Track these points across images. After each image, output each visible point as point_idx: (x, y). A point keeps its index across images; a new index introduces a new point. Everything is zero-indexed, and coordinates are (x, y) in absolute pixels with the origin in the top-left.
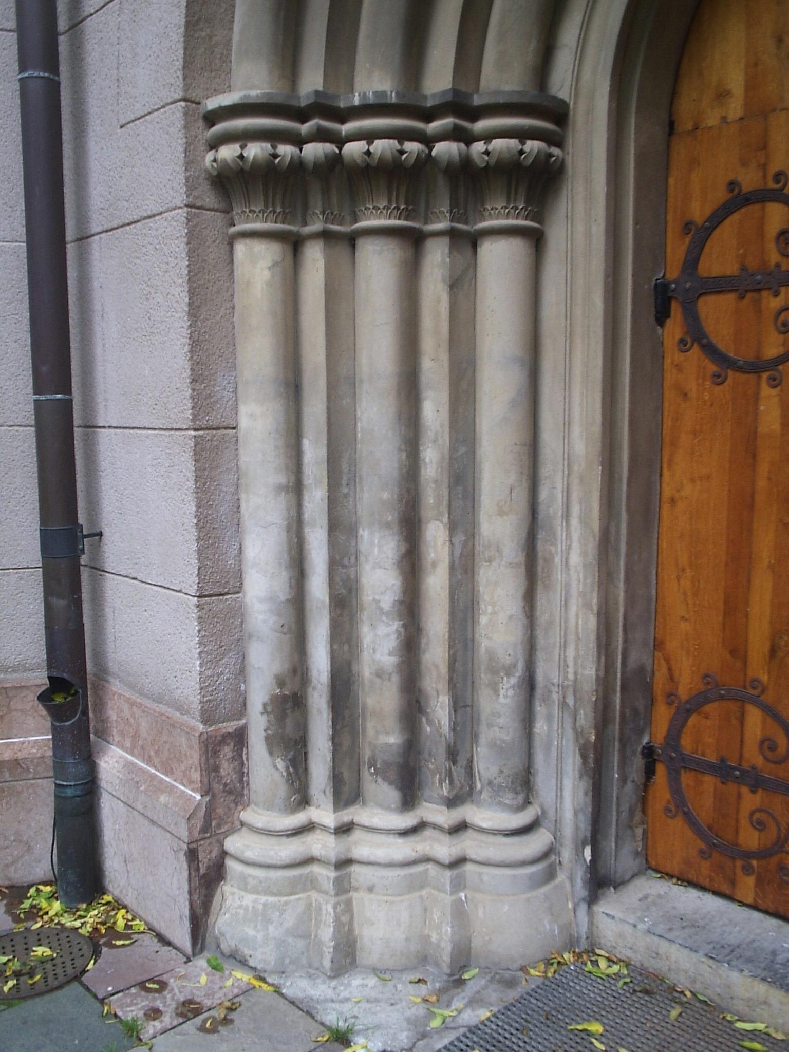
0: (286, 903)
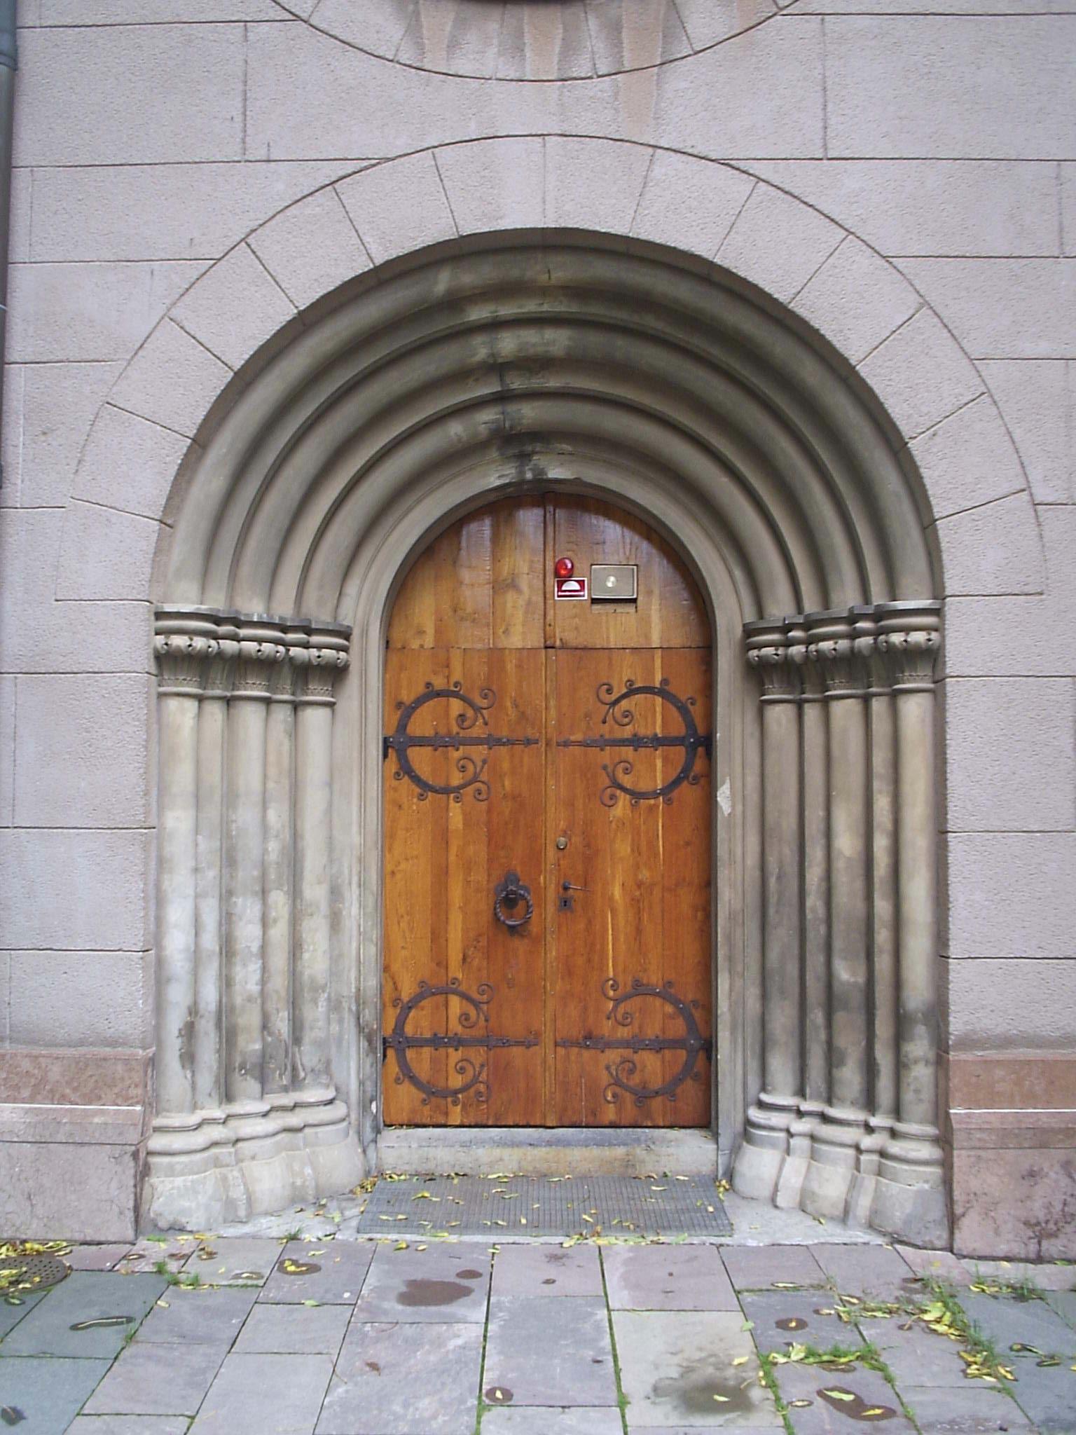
0: (205, 1177)
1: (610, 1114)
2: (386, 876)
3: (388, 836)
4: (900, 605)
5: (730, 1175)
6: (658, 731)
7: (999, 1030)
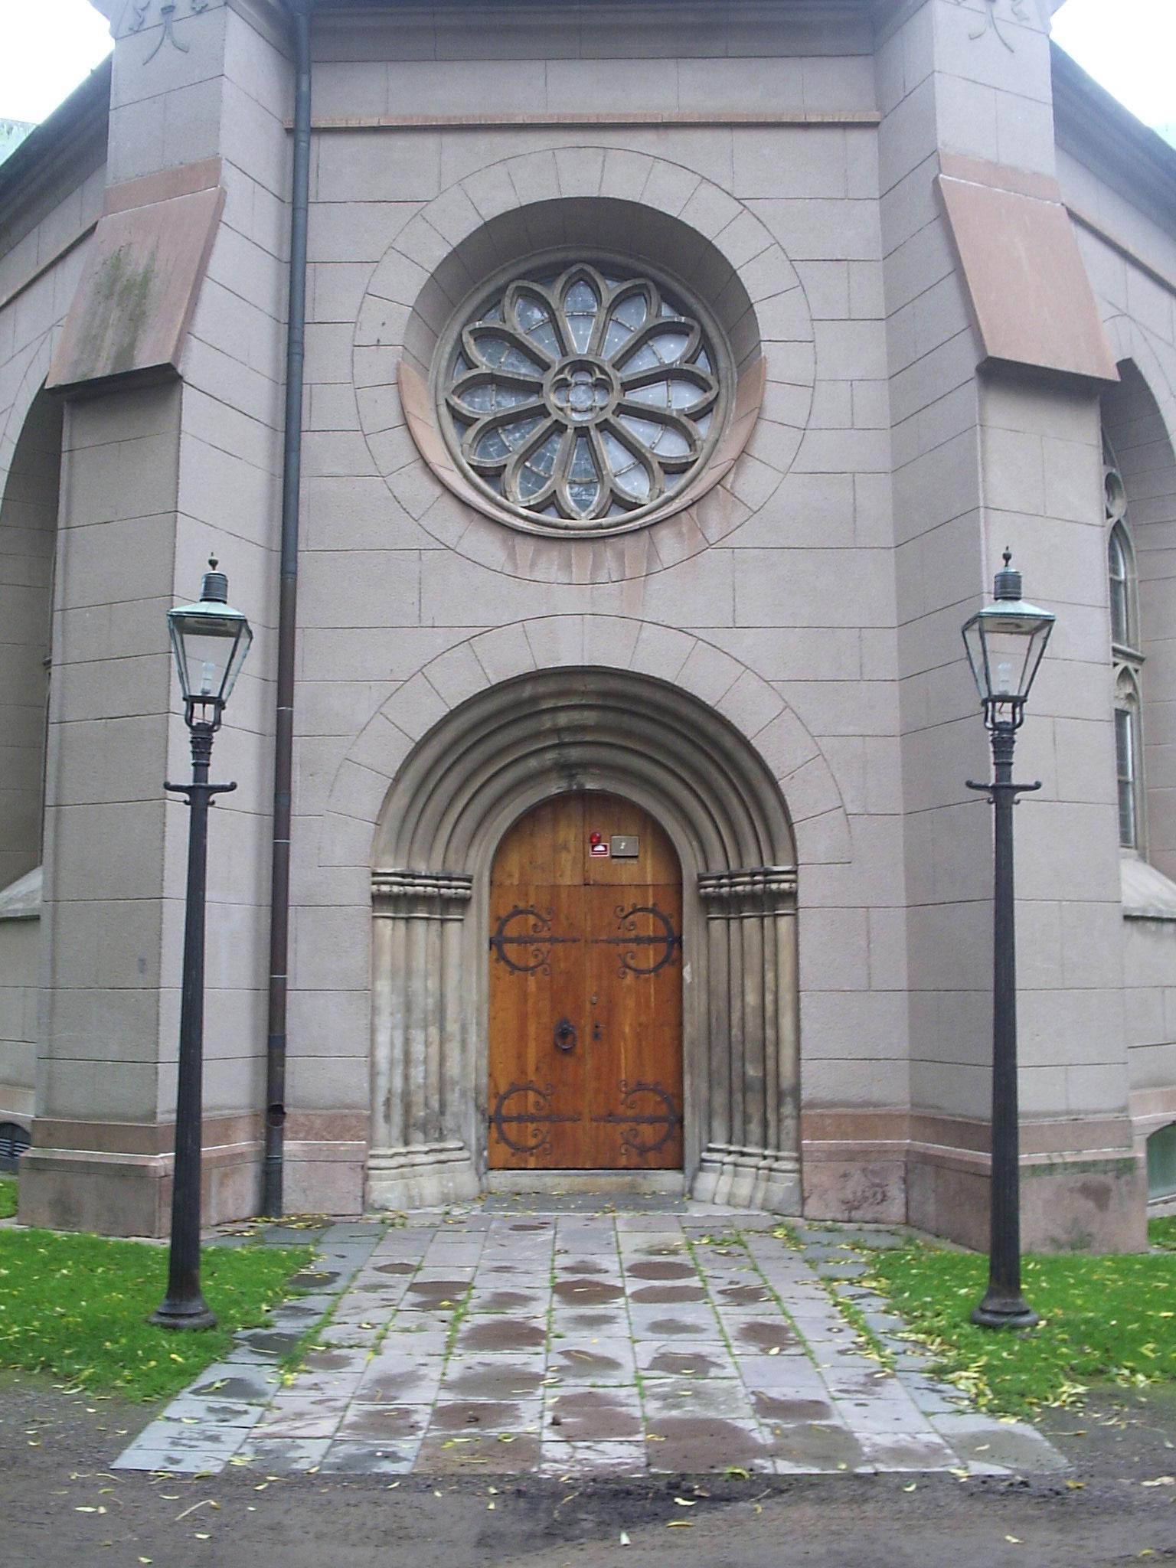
1: (623, 1161)
2: (492, 1019)
3: (493, 996)
4: (776, 869)
5: (691, 1190)
6: (651, 934)
7: (828, 1099)
